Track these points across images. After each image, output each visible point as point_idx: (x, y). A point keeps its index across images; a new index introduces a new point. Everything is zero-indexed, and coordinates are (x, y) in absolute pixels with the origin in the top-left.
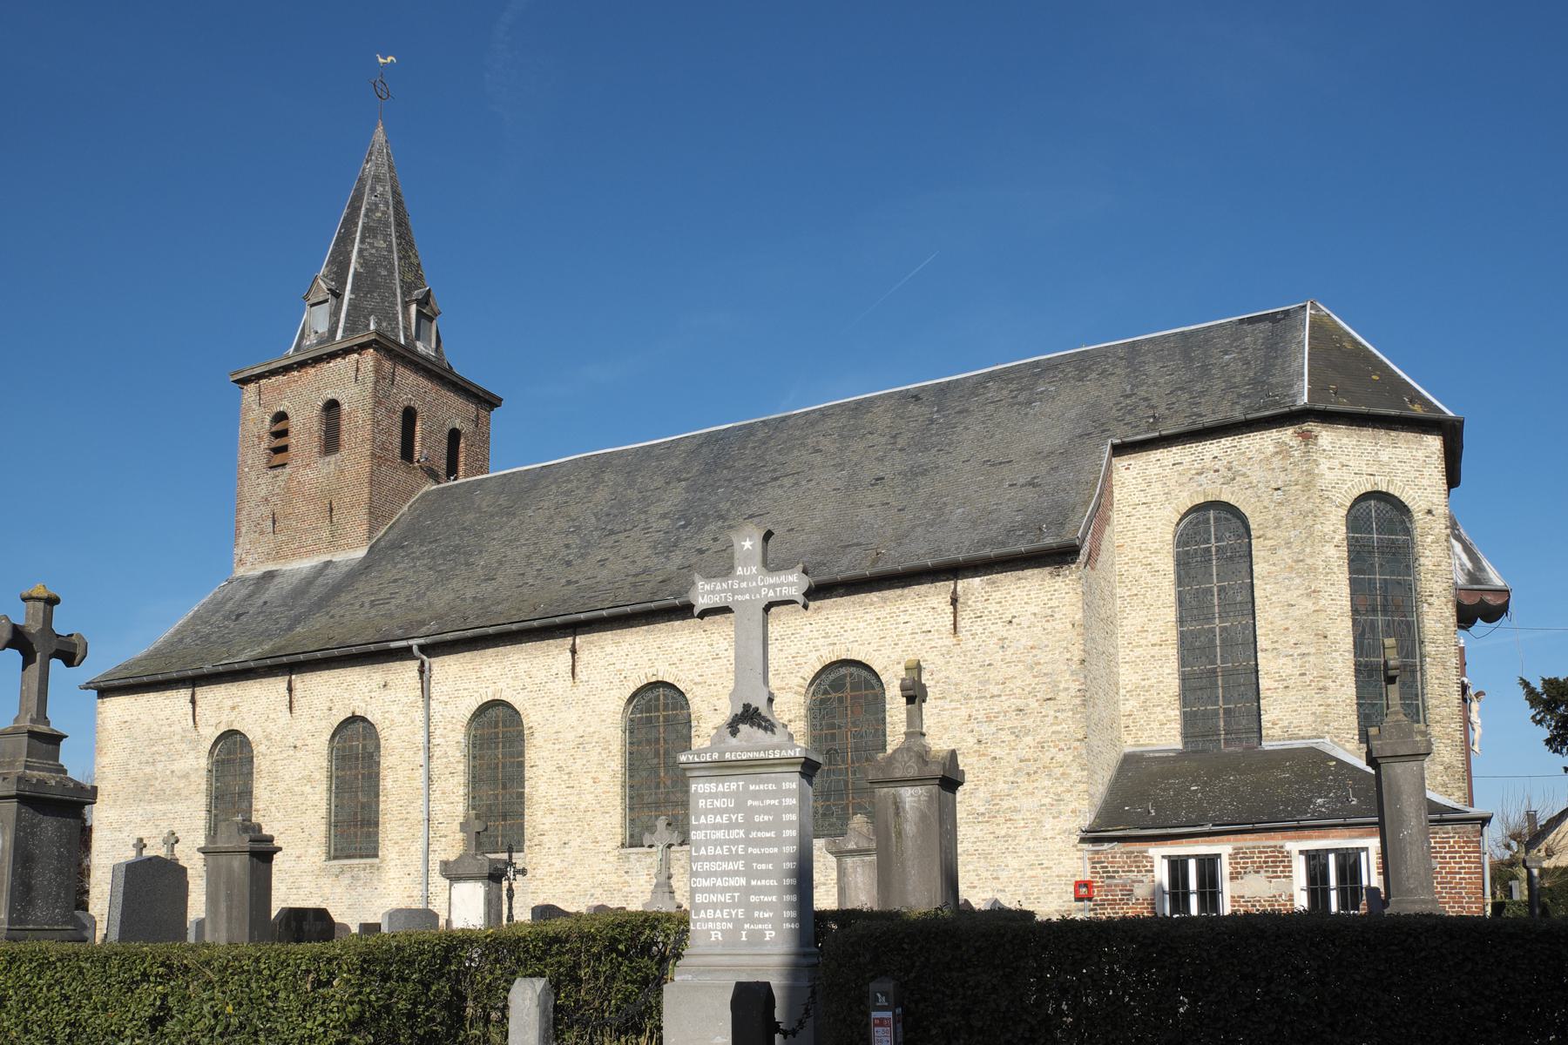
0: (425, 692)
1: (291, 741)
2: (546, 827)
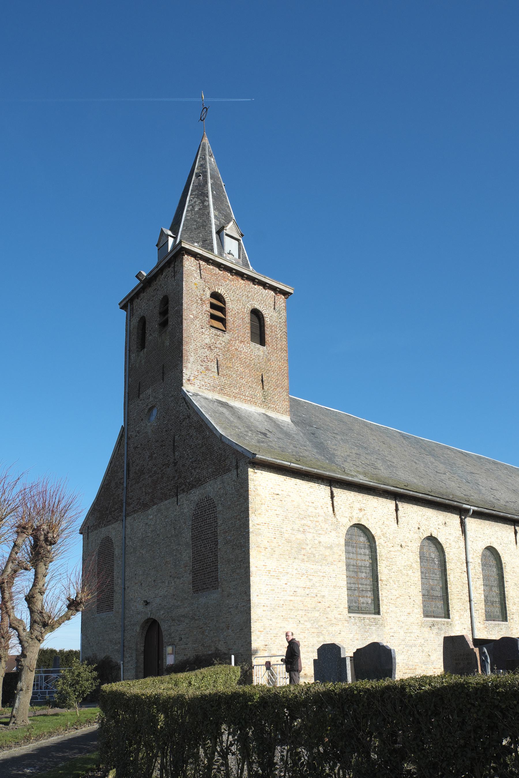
0: (464, 532)
1: (398, 541)
2: (514, 611)
